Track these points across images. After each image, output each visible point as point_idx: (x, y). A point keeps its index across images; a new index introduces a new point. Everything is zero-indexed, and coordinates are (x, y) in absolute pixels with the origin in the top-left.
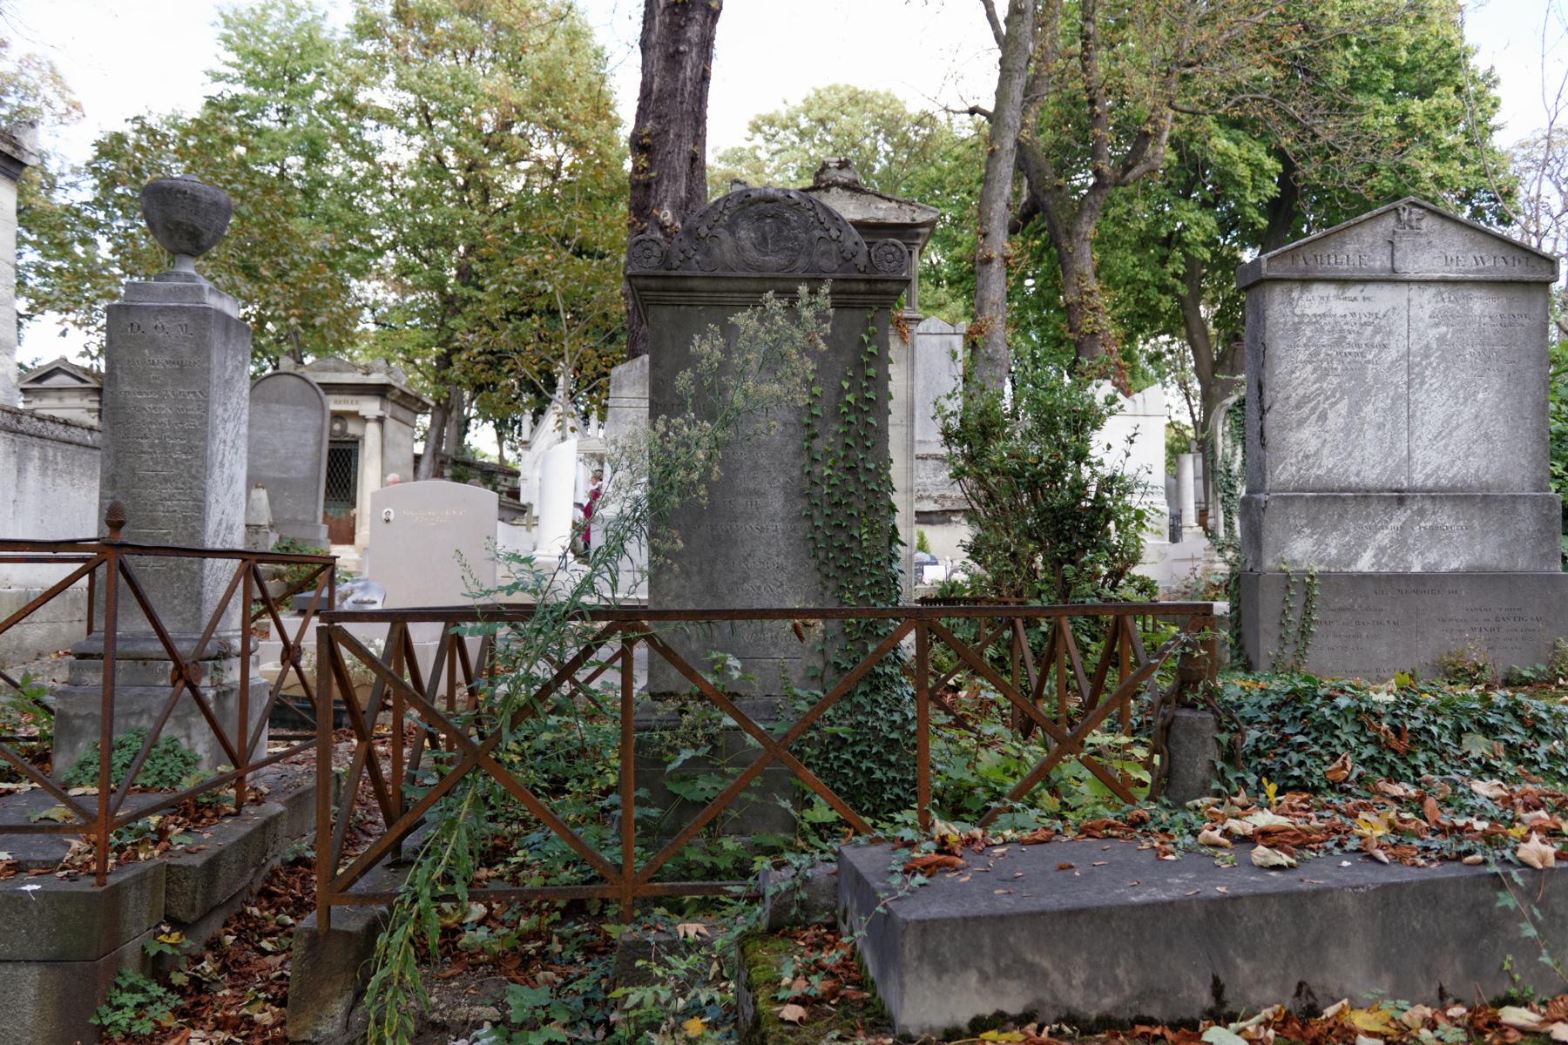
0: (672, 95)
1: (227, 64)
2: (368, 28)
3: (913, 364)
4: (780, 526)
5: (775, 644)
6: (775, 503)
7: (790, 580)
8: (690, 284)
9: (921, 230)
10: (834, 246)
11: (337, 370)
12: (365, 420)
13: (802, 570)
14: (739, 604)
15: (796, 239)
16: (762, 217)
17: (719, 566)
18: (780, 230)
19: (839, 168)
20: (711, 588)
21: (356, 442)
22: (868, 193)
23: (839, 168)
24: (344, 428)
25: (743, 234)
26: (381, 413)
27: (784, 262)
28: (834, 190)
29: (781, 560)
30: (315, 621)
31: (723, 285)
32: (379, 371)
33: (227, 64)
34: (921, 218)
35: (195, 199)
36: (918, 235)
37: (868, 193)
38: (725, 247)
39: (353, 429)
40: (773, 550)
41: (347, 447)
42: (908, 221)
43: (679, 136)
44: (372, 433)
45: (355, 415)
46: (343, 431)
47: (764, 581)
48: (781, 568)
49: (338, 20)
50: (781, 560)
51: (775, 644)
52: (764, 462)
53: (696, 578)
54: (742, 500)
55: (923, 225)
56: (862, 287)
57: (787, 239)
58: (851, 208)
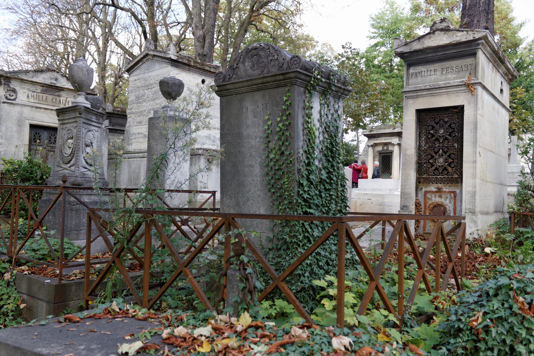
0: (475, 5)
1: (373, 33)
2: (416, 9)
3: (477, 104)
4: (259, 179)
5: (257, 227)
6: (257, 170)
7: (262, 201)
8: (228, 87)
9: (479, 42)
10: (276, 62)
11: (384, 129)
12: (394, 145)
13: (266, 197)
14: (246, 212)
15: (263, 62)
16: (253, 56)
17: (240, 195)
18: (259, 60)
19: (441, 22)
20: (238, 204)
21: (392, 152)
22: (452, 30)
23: (441, 22)
24: (388, 148)
25: (247, 64)
26: (399, 142)
27: (260, 72)
28: (437, 33)
29: (259, 193)
30: (422, 213)
31: (237, 86)
32: (398, 127)
33: (373, 33)
34: (477, 36)
35: (168, 83)
36: (479, 44)
37: (452, 30)
38: (242, 71)
39: (390, 148)
40: (257, 189)
41: (389, 154)
42: (471, 38)
43: (478, 21)
44: (396, 149)
45: (390, 143)
46: (387, 149)
47: (254, 201)
48: (259, 196)
49: (406, 10)
50: (259, 193)
51: (257, 227)
52: (254, 153)
53: (233, 200)
54: (247, 169)
55: (479, 39)
56: (281, 77)
57: (261, 63)
58: (444, 39)
